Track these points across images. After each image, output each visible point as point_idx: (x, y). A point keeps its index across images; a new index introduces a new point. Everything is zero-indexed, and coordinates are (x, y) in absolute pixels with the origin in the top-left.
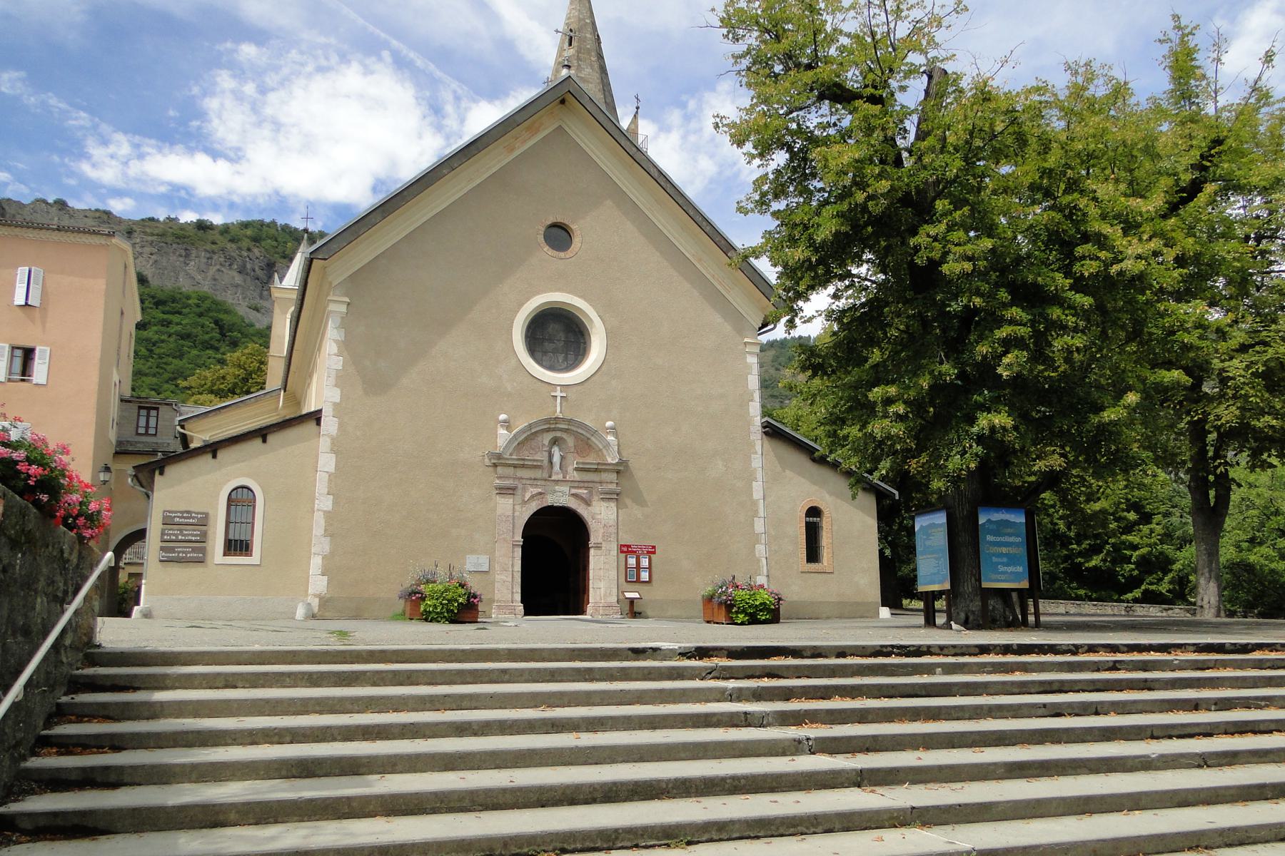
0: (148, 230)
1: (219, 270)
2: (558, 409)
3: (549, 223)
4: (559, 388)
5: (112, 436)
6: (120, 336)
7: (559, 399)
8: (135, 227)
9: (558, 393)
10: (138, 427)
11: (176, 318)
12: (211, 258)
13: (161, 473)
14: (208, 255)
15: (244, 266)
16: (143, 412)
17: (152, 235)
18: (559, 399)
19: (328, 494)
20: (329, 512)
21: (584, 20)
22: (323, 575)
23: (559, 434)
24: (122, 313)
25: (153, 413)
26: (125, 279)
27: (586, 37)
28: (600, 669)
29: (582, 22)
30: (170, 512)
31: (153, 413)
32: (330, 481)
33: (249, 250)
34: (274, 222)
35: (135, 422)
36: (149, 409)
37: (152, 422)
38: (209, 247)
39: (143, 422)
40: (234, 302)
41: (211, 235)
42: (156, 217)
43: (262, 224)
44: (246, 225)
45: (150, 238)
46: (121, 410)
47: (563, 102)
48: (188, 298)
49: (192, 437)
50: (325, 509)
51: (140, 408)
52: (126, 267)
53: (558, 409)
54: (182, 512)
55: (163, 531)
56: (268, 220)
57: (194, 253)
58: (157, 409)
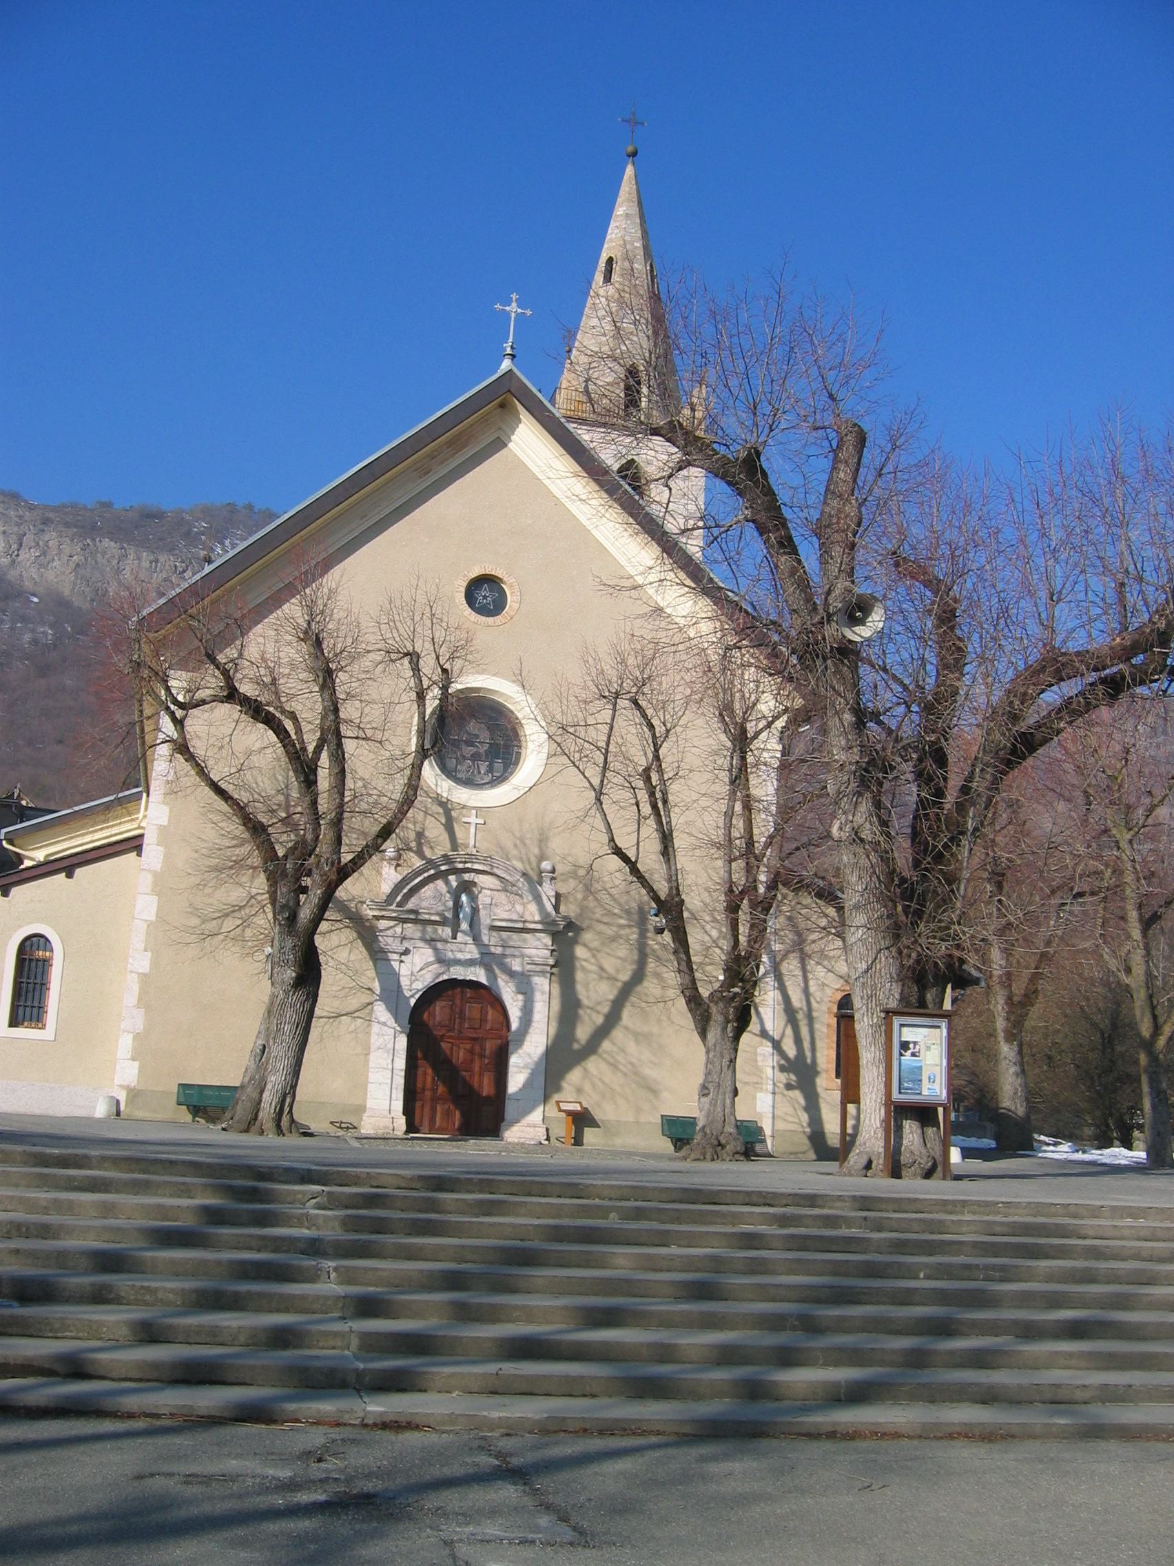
1: (165, 580)
19: (145, 950)
22: (133, 1059)
32: (148, 933)
53: (472, 843)
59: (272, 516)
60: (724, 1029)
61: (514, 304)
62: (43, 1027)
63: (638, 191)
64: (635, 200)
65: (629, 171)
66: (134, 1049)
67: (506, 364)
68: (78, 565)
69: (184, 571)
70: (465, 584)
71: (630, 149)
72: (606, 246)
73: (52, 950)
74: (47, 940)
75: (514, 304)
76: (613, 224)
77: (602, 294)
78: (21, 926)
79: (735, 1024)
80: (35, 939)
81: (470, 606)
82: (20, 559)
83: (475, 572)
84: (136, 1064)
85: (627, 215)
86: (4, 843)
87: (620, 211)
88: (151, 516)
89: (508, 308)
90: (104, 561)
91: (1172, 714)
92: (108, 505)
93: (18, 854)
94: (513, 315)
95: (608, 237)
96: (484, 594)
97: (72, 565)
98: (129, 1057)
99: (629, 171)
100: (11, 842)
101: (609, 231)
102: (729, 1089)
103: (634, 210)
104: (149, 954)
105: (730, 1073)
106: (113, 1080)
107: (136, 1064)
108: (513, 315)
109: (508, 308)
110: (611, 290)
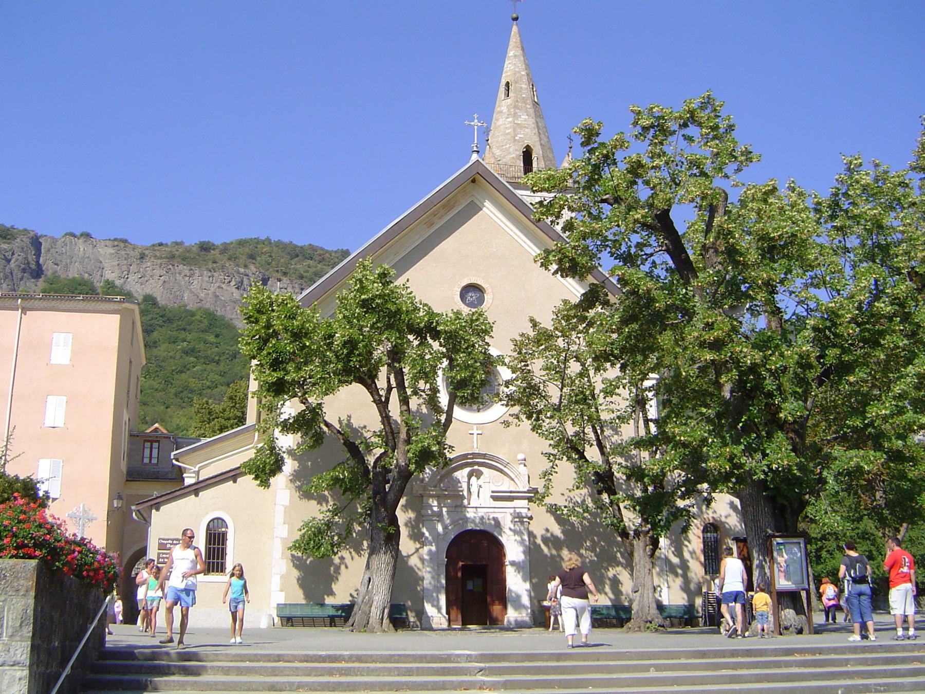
0: (158, 254)
1: (219, 287)
2: (475, 447)
3: (464, 284)
4: (475, 427)
5: (123, 467)
6: (129, 386)
7: (475, 435)
8: (147, 252)
9: (475, 432)
10: (143, 458)
11: (183, 335)
12: (213, 276)
13: (158, 509)
14: (210, 274)
15: (242, 282)
16: (148, 445)
17: (161, 258)
18: (475, 435)
19: (284, 523)
20: (285, 539)
21: (519, 72)
22: (281, 591)
23: (476, 467)
24: (131, 362)
25: (156, 445)
26: (133, 334)
27: (521, 88)
28: (77, 647)
29: (518, 75)
30: (163, 540)
31: (156, 445)
32: (285, 512)
33: (246, 266)
34: (268, 239)
35: (141, 453)
36: (152, 442)
37: (155, 452)
38: (210, 266)
39: (147, 452)
40: (233, 317)
41: (215, 253)
42: (164, 242)
43: (258, 241)
44: (241, 243)
45: (159, 261)
46: (131, 443)
47: (474, 181)
48: (193, 315)
49: (185, 468)
50: (282, 536)
51: (145, 441)
52: (133, 323)
53: (475, 447)
54: (173, 540)
55: (159, 554)
56: (263, 238)
57: (197, 273)
58: (158, 441)
59: (346, 253)
60: (645, 550)
61: (476, 121)
62: (497, 524)
63: (521, 41)
64: (520, 46)
65: (515, 29)
66: (282, 584)
67: (475, 157)
68: (165, 282)
69: (230, 282)
70: (460, 290)
71: (514, 16)
72: (504, 75)
73: (227, 527)
74: (223, 520)
75: (476, 121)
76: (507, 62)
77: (503, 105)
78: (207, 513)
79: (651, 547)
80: (220, 521)
81: (462, 301)
82: (129, 280)
83: (479, 282)
84: (283, 593)
85: (515, 56)
86: (174, 461)
87: (511, 53)
88: (205, 247)
89: (472, 123)
90: (181, 278)
91: (0, 270)
92: (182, 243)
93: (180, 467)
94: (476, 127)
95: (505, 70)
96: (472, 296)
97: (161, 282)
98: (279, 589)
99: (515, 29)
100: (177, 460)
101: (505, 66)
102: (651, 587)
103: (520, 52)
104: (287, 526)
105: (650, 577)
106: (269, 604)
107: (283, 593)
108: (476, 127)
109: (472, 123)
110: (509, 101)
